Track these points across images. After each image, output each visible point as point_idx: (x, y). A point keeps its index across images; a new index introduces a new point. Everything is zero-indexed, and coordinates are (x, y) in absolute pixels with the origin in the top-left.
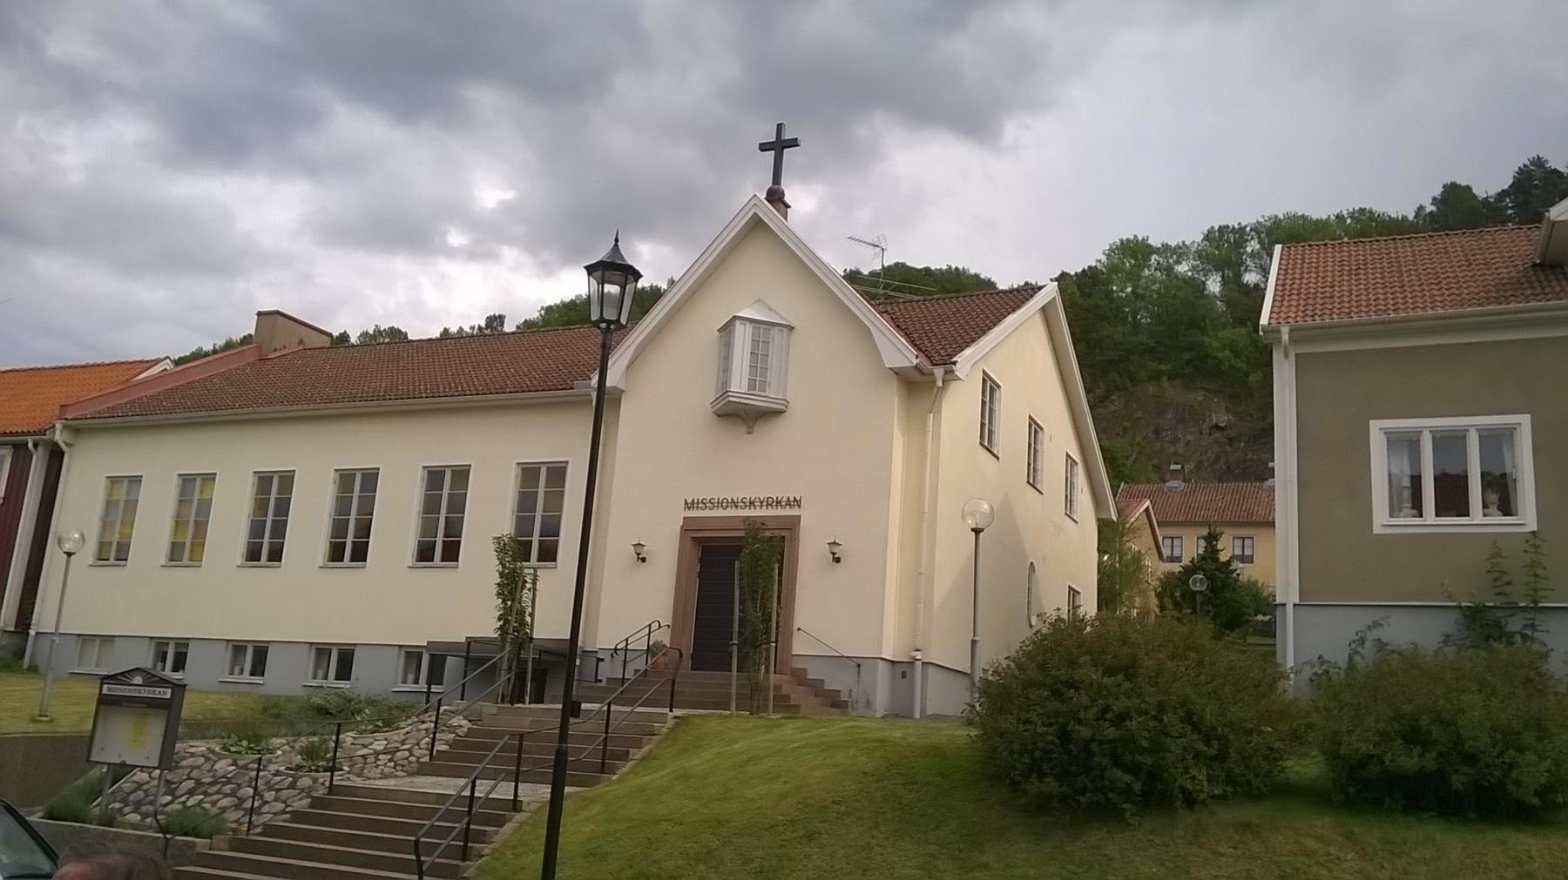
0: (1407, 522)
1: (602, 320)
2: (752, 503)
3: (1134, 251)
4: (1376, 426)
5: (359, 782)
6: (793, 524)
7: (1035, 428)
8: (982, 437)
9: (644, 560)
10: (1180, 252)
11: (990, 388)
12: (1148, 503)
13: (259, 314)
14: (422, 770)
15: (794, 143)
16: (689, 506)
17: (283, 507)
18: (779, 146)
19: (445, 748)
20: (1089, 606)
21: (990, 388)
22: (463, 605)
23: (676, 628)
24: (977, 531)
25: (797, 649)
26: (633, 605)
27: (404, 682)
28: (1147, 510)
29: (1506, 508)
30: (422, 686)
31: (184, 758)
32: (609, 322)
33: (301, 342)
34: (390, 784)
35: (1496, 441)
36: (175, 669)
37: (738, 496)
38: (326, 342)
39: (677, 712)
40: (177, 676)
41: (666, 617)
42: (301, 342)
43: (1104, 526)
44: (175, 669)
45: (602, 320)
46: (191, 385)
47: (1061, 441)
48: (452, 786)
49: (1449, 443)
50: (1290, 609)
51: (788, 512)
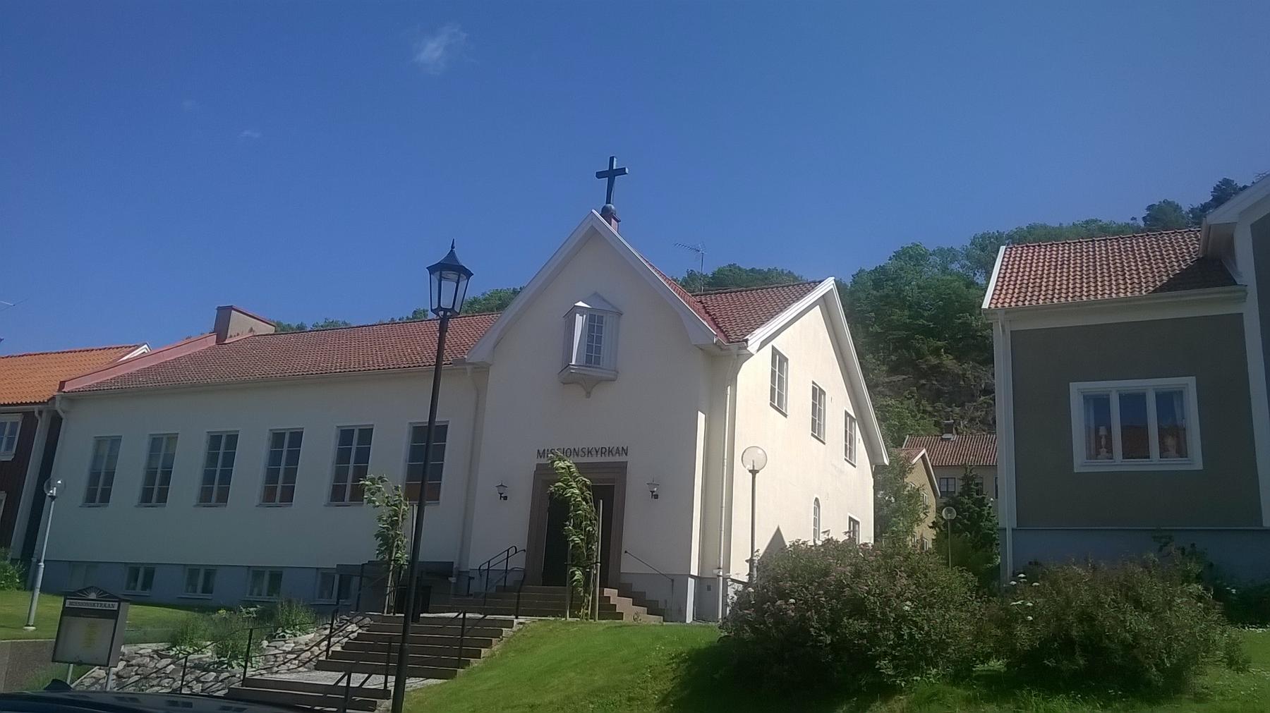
0: (1101, 466)
1: (440, 308)
2: (589, 452)
3: (912, 256)
4: (1075, 387)
5: (268, 677)
6: (622, 467)
7: (818, 394)
8: (772, 399)
9: (505, 498)
10: (947, 255)
11: (779, 360)
12: (924, 451)
13: (219, 309)
14: (320, 666)
15: (622, 171)
16: (541, 454)
17: (229, 459)
18: (611, 175)
19: (339, 649)
20: (866, 535)
21: (779, 360)
22: (349, 537)
23: (530, 552)
24: (754, 472)
25: (624, 568)
26: (493, 530)
27: (321, 596)
28: (923, 457)
29: (1182, 452)
30: (334, 600)
31: (134, 658)
32: (446, 310)
33: (251, 330)
34: (292, 677)
35: (1167, 401)
36: (145, 587)
37: (579, 446)
38: (271, 330)
39: (522, 619)
40: (147, 593)
41: (522, 543)
42: (251, 330)
43: (878, 470)
44: (145, 587)
45: (440, 308)
46: (164, 365)
47: (839, 404)
48: (328, 678)
49: (1133, 403)
50: (1009, 533)
51: (617, 459)
